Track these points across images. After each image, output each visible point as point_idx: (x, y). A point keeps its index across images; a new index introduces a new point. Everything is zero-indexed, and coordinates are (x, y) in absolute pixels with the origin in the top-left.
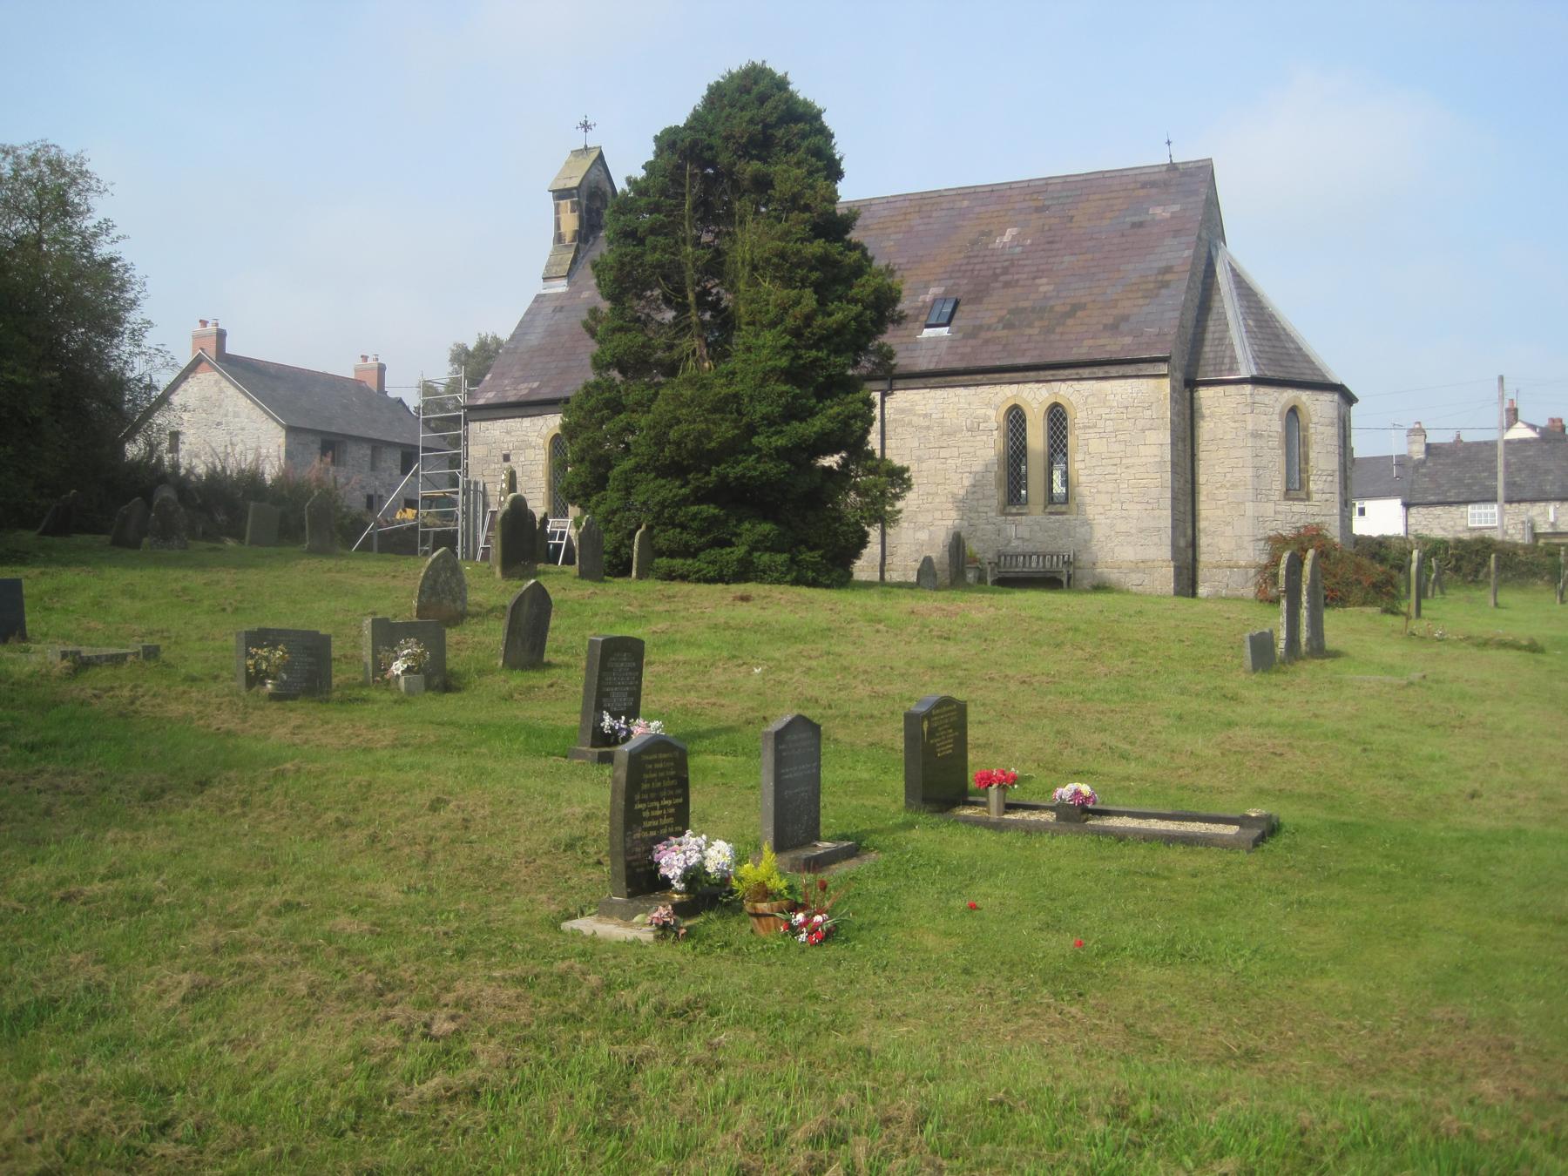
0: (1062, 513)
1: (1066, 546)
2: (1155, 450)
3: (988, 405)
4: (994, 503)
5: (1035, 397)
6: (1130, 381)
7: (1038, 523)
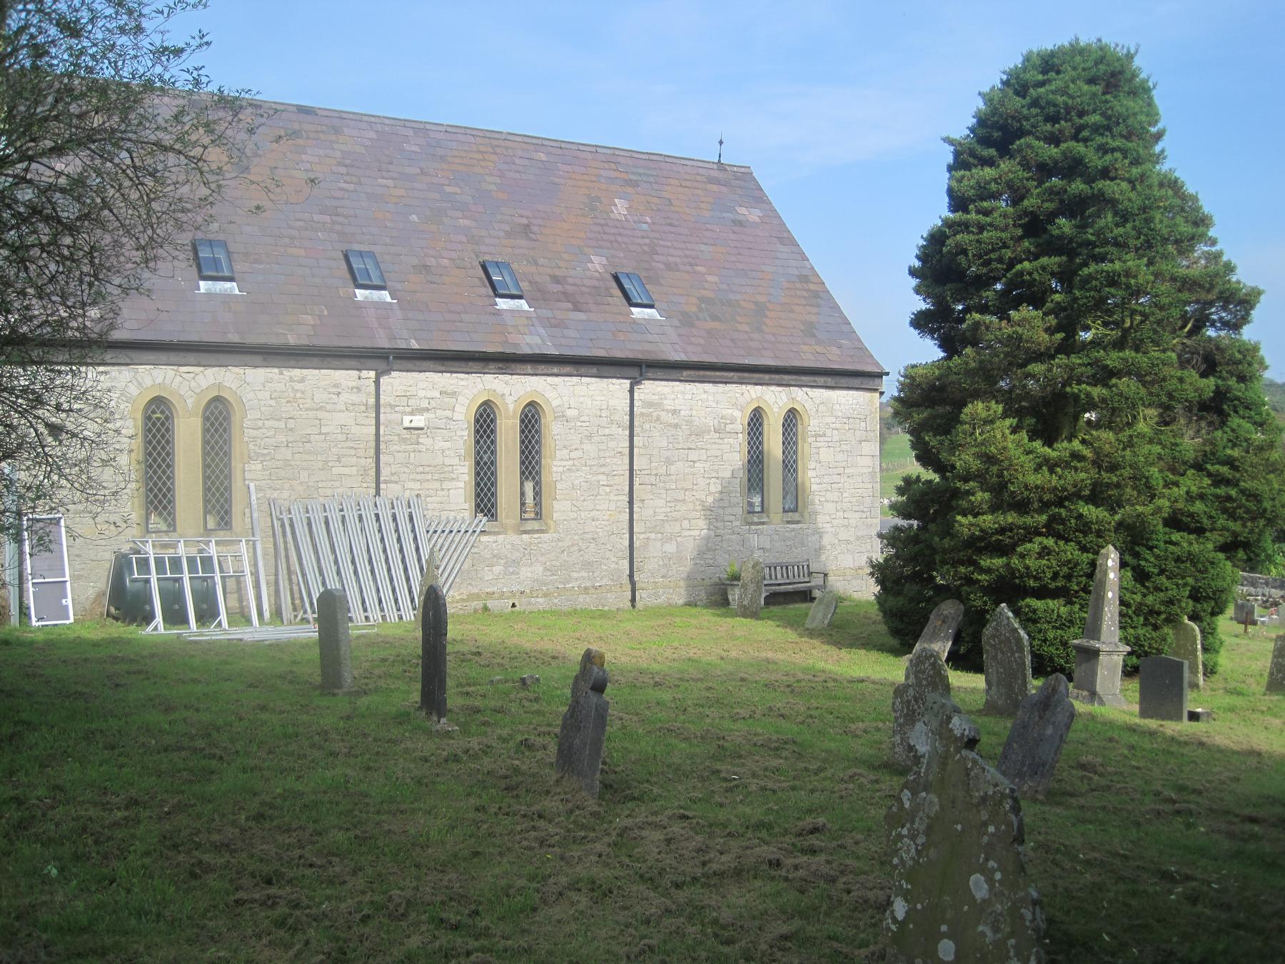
0: (798, 522)
2: (866, 461)
5: (776, 399)
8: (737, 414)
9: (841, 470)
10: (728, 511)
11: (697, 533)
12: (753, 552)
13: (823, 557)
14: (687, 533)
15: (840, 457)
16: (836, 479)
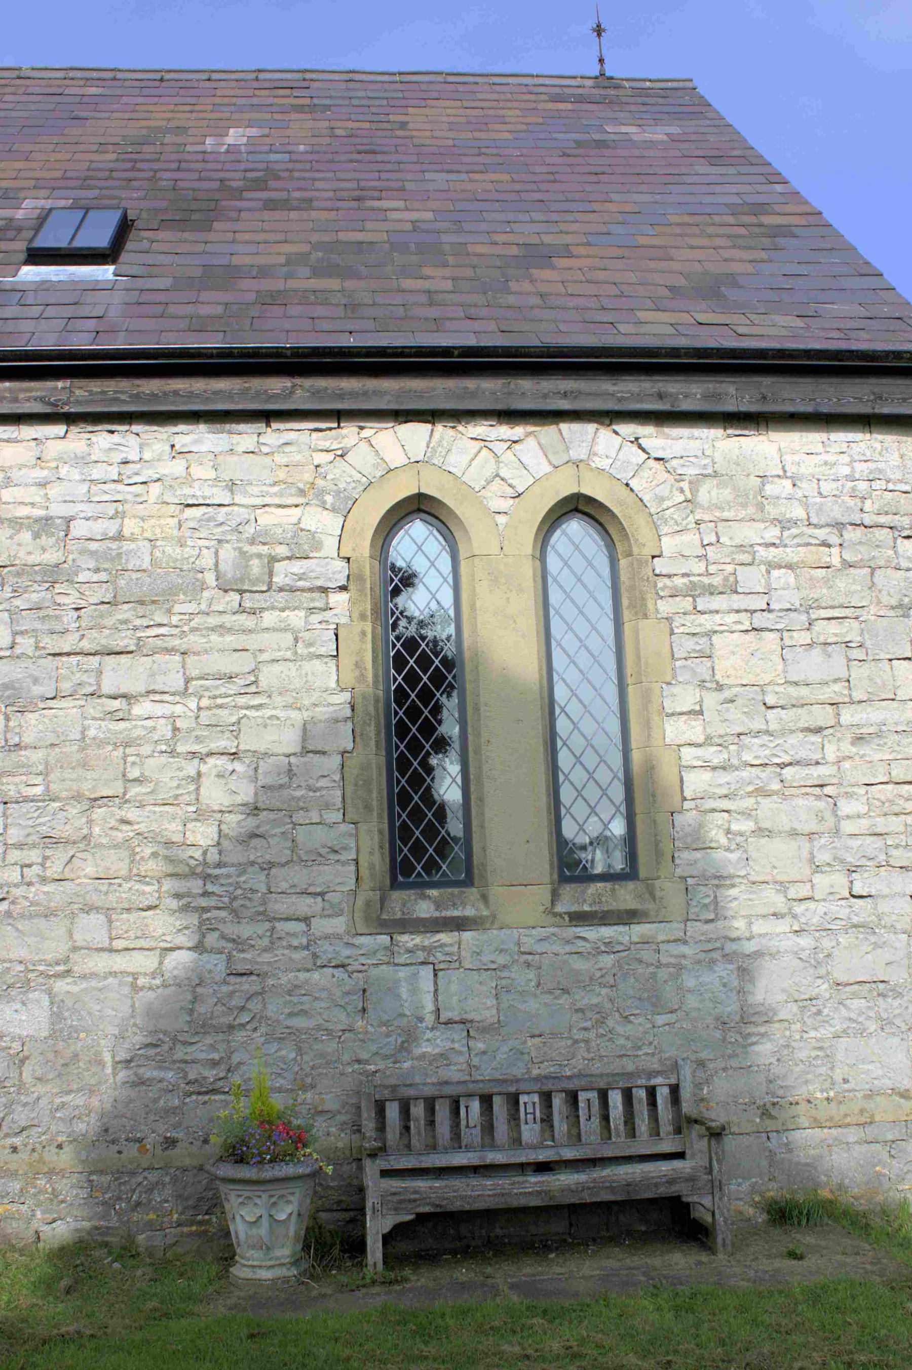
0: (629, 917)
1: (635, 1044)
3: (311, 494)
4: (339, 877)
5: (497, 468)
6: (840, 438)
7: (527, 958)
8: (323, 523)
9: (822, 716)
10: (285, 878)
11: (145, 962)
12: (410, 1037)
13: (764, 1052)
14: (101, 963)
15: (811, 665)
16: (798, 746)
